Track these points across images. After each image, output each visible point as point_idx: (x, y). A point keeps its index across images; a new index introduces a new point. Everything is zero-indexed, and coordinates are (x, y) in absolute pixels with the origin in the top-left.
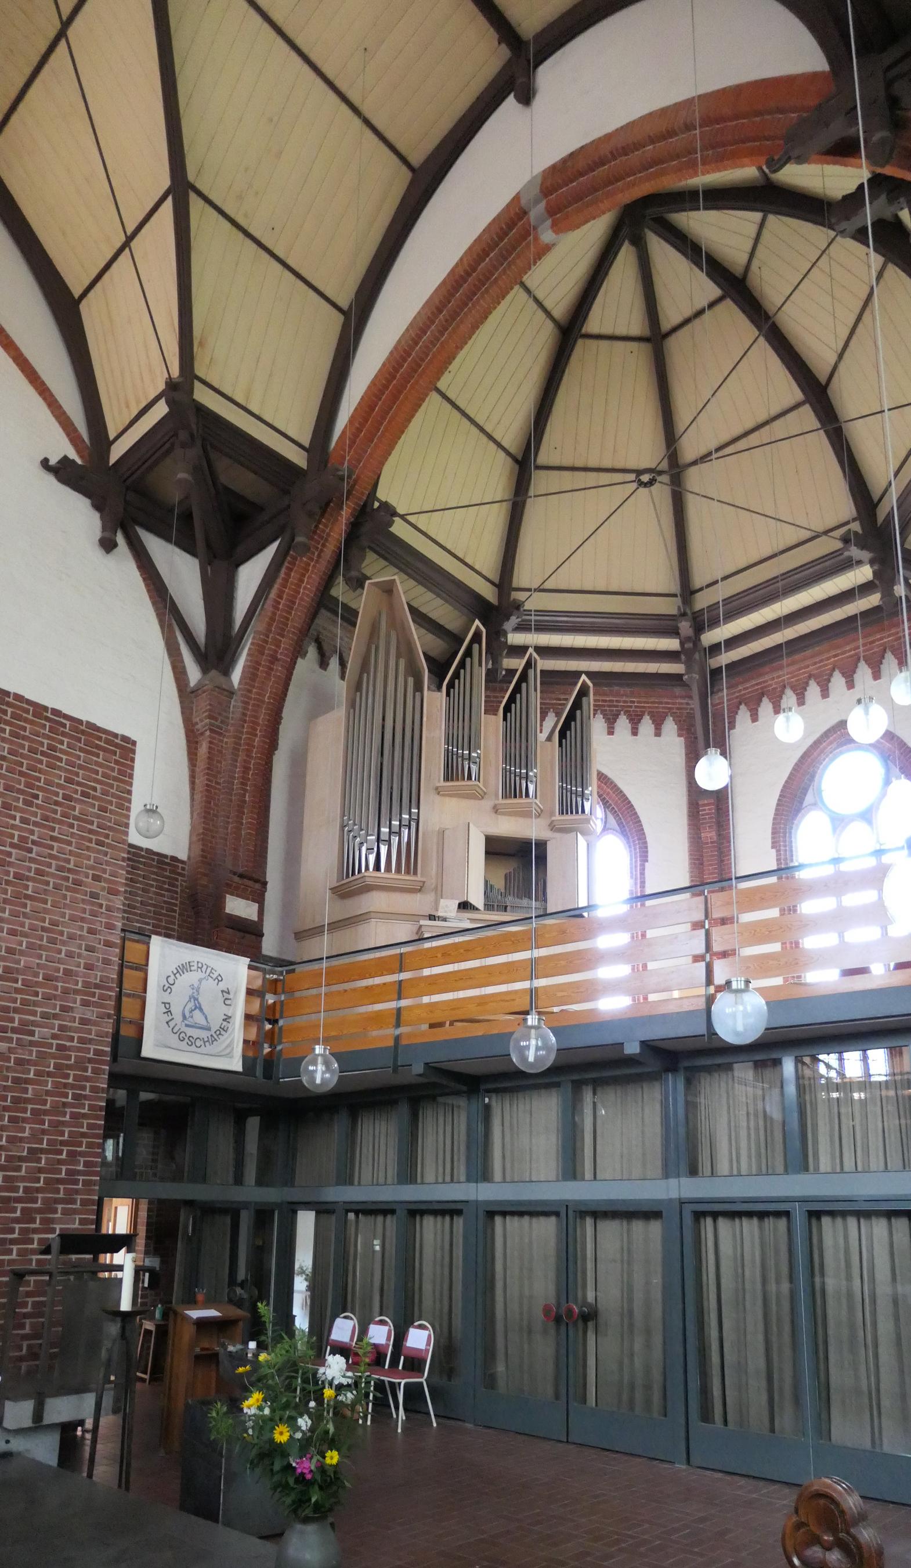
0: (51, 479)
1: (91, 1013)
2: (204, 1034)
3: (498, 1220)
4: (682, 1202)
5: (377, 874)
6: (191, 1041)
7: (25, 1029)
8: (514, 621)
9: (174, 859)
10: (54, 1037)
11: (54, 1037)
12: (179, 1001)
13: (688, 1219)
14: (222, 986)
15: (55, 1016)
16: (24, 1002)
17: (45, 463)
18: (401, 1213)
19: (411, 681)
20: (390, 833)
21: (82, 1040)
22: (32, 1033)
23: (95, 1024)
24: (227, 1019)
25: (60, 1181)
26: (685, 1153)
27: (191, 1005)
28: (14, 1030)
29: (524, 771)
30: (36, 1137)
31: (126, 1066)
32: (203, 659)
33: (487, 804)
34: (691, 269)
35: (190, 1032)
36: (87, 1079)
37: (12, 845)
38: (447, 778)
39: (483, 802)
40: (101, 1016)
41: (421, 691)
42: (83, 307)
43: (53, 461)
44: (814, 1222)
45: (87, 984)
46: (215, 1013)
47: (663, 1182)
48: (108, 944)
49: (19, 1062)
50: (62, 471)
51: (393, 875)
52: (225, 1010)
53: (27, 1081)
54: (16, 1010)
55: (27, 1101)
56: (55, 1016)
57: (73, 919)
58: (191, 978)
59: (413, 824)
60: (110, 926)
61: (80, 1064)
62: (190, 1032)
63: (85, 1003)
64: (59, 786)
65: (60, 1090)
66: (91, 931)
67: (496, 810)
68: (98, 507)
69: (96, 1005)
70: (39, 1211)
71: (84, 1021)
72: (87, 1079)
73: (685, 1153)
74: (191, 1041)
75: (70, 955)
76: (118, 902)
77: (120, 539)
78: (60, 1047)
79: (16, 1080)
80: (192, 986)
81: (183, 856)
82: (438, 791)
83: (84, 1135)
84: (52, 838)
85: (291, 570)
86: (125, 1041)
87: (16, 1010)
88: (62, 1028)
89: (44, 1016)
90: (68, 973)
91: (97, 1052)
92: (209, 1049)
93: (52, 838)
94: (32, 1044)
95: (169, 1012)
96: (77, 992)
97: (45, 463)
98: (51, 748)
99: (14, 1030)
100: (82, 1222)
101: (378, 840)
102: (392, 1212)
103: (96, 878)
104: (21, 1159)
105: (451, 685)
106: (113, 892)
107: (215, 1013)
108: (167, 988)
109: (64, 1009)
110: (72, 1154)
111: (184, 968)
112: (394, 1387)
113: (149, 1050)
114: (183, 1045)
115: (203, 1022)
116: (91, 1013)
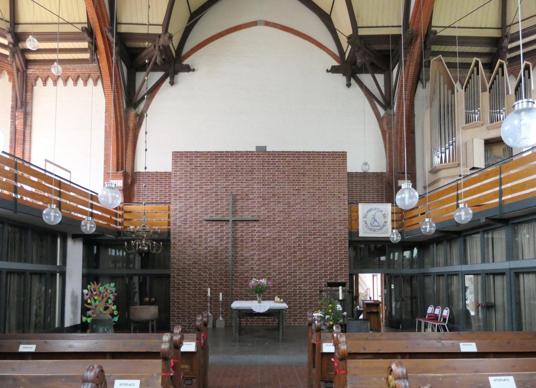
0: (330, 74)
1: (342, 228)
2: (378, 228)
3: (521, 276)
4: (511, 269)
5: (446, 164)
6: (374, 230)
7: (325, 234)
8: (506, 41)
9: (382, 173)
10: (333, 235)
11: (333, 235)
12: (369, 220)
13: (513, 275)
14: (383, 213)
15: (332, 230)
16: (324, 228)
17: (327, 71)
18: (445, 276)
19: (450, 91)
20: (445, 149)
21: (340, 235)
22: (327, 235)
23: (343, 230)
24: (386, 222)
25: (338, 270)
26: (512, 252)
27: (373, 220)
28: (322, 235)
29: (498, 111)
30: (331, 260)
31: (354, 239)
32: (385, 107)
33: (484, 127)
34: (358, 17)
35: (375, 228)
36: (343, 244)
37: (317, 190)
38: (466, 123)
39: (483, 127)
40: (345, 228)
41: (454, 94)
42: (332, 16)
43: (329, 69)
44: (449, 277)
45: (339, 220)
46: (381, 221)
47: (508, 262)
48: (344, 209)
49: (324, 242)
50: (334, 70)
51: (451, 163)
52: (384, 220)
53: (327, 247)
54: (322, 230)
55: (328, 251)
56: (332, 230)
57: (334, 204)
58: (373, 213)
59: (454, 143)
60: (344, 204)
61: (340, 241)
62: (373, 228)
63: (340, 225)
64: (327, 171)
65: (335, 248)
66: (340, 207)
67: (488, 129)
68: (344, 75)
69: (343, 225)
70: (334, 277)
71: (340, 230)
72: (343, 244)
73: (512, 252)
74: (374, 230)
75: (334, 214)
76: (346, 197)
77: (353, 81)
78: (334, 237)
79: (324, 247)
80: (373, 215)
81: (385, 171)
82: (463, 128)
83: (343, 259)
84: (327, 185)
85: (410, 66)
86: (353, 233)
87: (322, 230)
88: (334, 232)
89: (329, 230)
90: (334, 218)
91: (345, 237)
92: (380, 232)
93: (327, 185)
94: (327, 237)
95: (366, 223)
96: (337, 223)
97: (327, 71)
98: (323, 162)
99: (322, 235)
100: (345, 280)
101: (441, 153)
102: (480, 274)
103: (339, 192)
104: (328, 265)
105: (466, 87)
106: (344, 195)
107: (381, 221)
108: (365, 217)
109: (334, 228)
110: (341, 264)
111: (370, 210)
112: (435, 325)
113: (361, 234)
114: (372, 232)
115: (377, 224)
116: (342, 228)
